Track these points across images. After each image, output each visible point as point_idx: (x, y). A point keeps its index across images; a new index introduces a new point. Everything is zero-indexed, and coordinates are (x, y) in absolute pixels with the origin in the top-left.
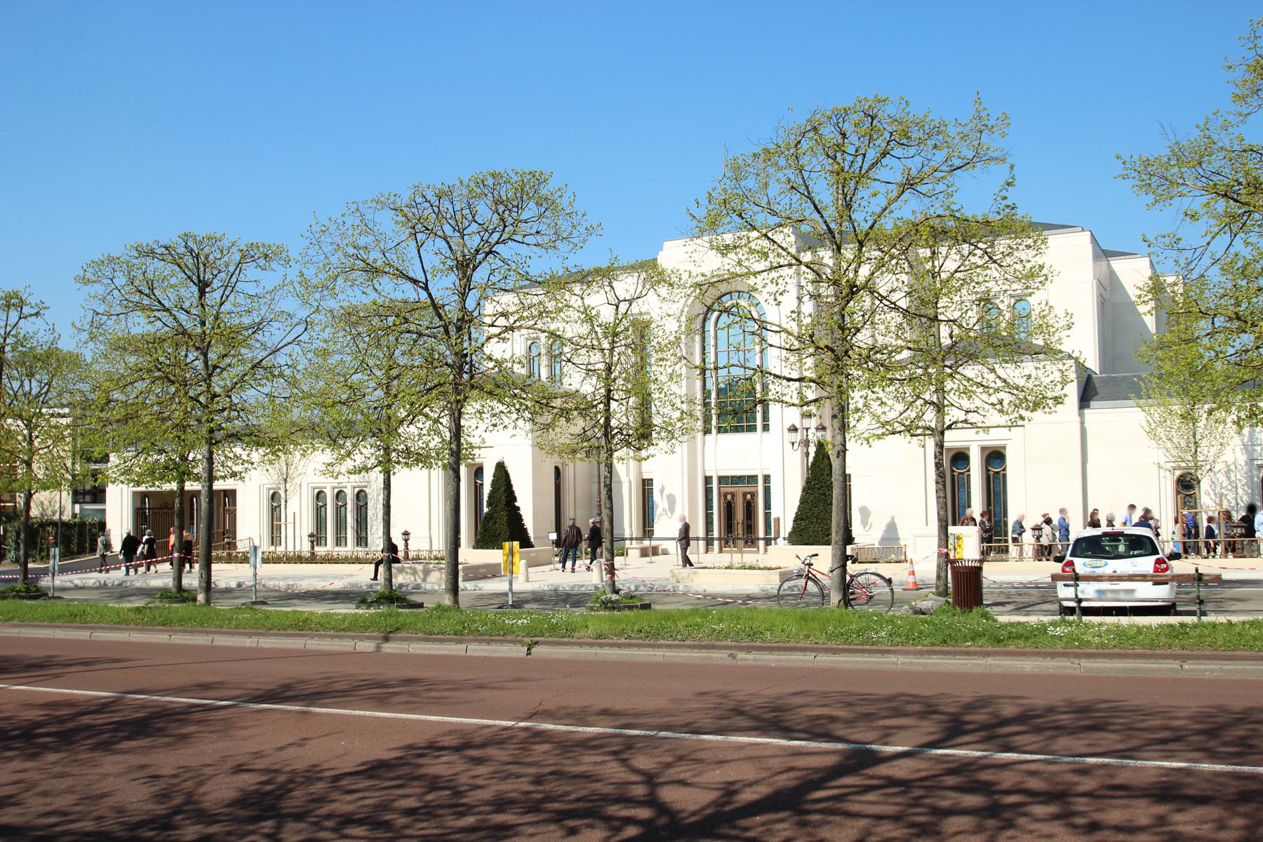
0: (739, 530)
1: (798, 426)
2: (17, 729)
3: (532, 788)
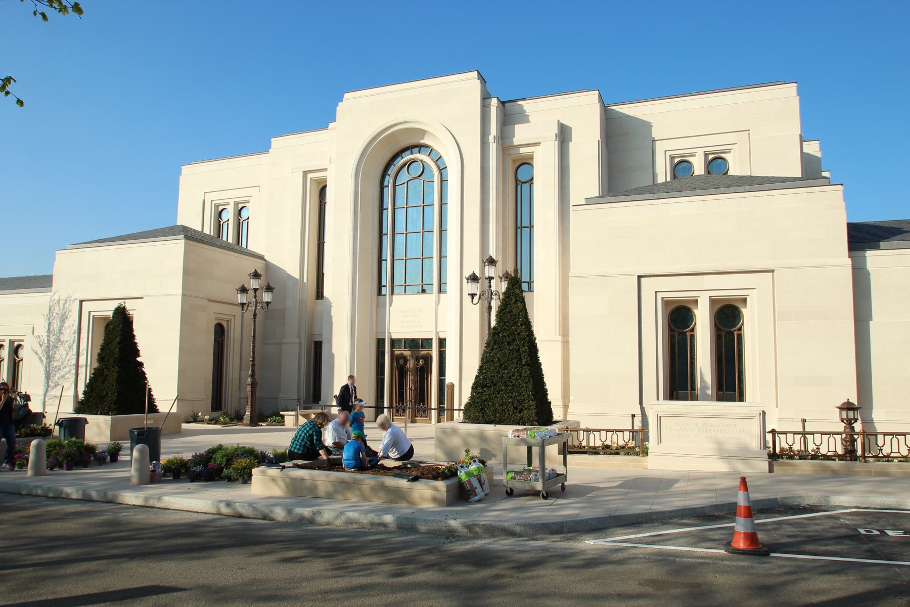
0: (409, 395)
1: (478, 274)
2: (332, 599)
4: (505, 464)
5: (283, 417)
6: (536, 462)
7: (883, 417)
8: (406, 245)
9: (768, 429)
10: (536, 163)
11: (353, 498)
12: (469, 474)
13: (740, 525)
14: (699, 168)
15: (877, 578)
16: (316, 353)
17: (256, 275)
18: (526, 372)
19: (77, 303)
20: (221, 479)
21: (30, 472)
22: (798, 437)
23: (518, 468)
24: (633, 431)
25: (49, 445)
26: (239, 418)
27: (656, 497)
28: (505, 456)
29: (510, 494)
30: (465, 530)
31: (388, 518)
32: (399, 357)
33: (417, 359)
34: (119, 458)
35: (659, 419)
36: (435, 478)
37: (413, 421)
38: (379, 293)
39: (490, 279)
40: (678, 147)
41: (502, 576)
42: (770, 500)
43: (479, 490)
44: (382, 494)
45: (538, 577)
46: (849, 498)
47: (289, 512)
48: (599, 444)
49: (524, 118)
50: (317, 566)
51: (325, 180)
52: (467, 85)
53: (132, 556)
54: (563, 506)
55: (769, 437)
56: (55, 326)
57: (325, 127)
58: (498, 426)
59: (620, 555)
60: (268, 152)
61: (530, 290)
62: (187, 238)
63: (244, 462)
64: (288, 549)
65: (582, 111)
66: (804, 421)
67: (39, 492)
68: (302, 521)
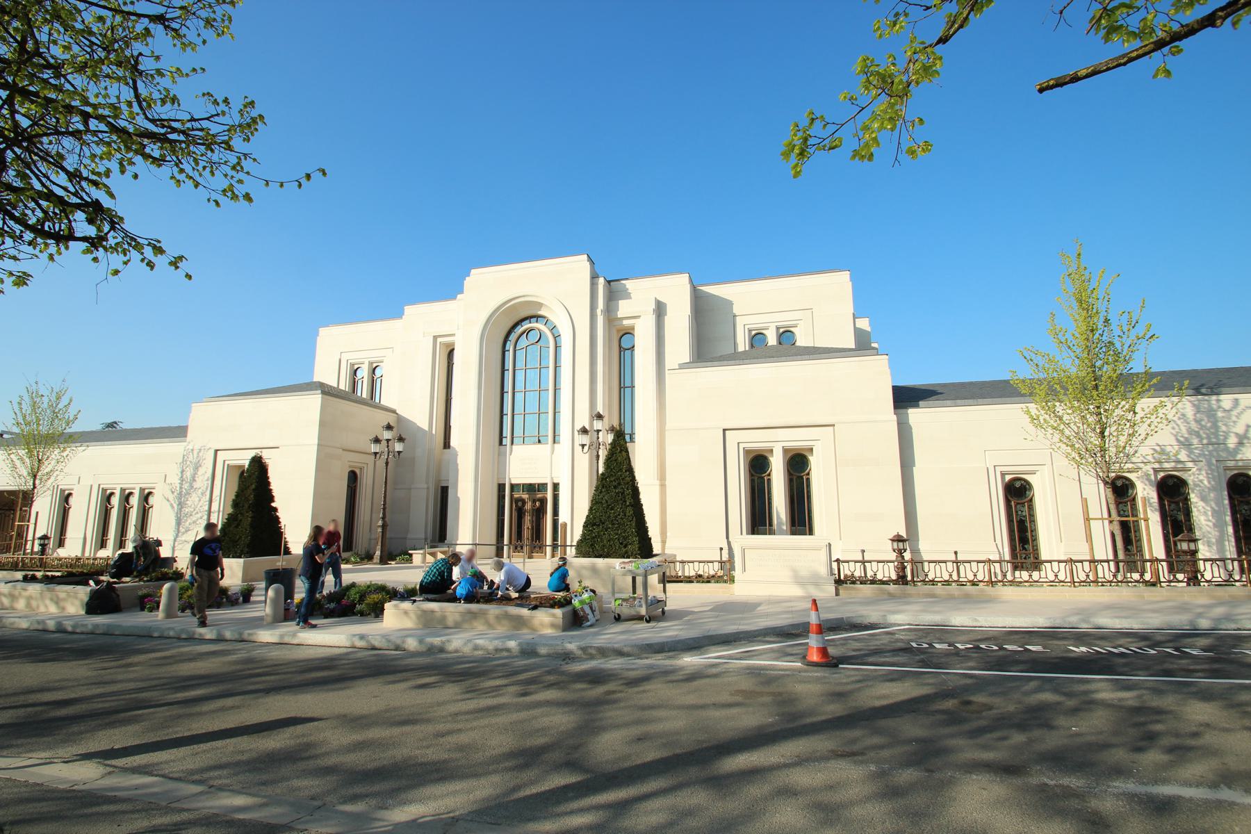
0: (526, 534)
3: (1167, 702)
4: (613, 593)
5: (411, 555)
6: (640, 590)
7: (929, 547)
8: (524, 402)
9: (834, 558)
10: (636, 333)
11: (480, 626)
12: (582, 602)
13: (813, 641)
14: (772, 340)
15: (929, 684)
16: (443, 497)
17: (389, 427)
18: (630, 511)
19: (212, 453)
20: (354, 614)
21: (160, 614)
22: (858, 565)
23: (625, 596)
24: (721, 562)
25: (181, 589)
26: (369, 557)
27: (742, 619)
28: (613, 584)
29: (618, 619)
30: (580, 652)
31: (512, 644)
32: (518, 500)
33: (534, 501)
34: (252, 599)
35: (743, 551)
36: (552, 606)
37: (530, 557)
38: (501, 443)
39: (598, 431)
40: (755, 322)
41: (614, 692)
42: (837, 619)
43: (590, 616)
44: (505, 622)
45: (644, 691)
46: (904, 617)
47: (421, 642)
48: (692, 573)
49: (627, 296)
50: (450, 691)
51: (453, 344)
52: (578, 266)
53: (268, 691)
54: (666, 629)
55: (835, 565)
56: (188, 474)
57: (454, 298)
58: (607, 560)
59: (714, 671)
60: (401, 317)
61: (632, 440)
62: (323, 393)
63: (376, 597)
64: (420, 676)
65: (675, 290)
66: (956, 553)
67: (172, 633)
68: (432, 650)
